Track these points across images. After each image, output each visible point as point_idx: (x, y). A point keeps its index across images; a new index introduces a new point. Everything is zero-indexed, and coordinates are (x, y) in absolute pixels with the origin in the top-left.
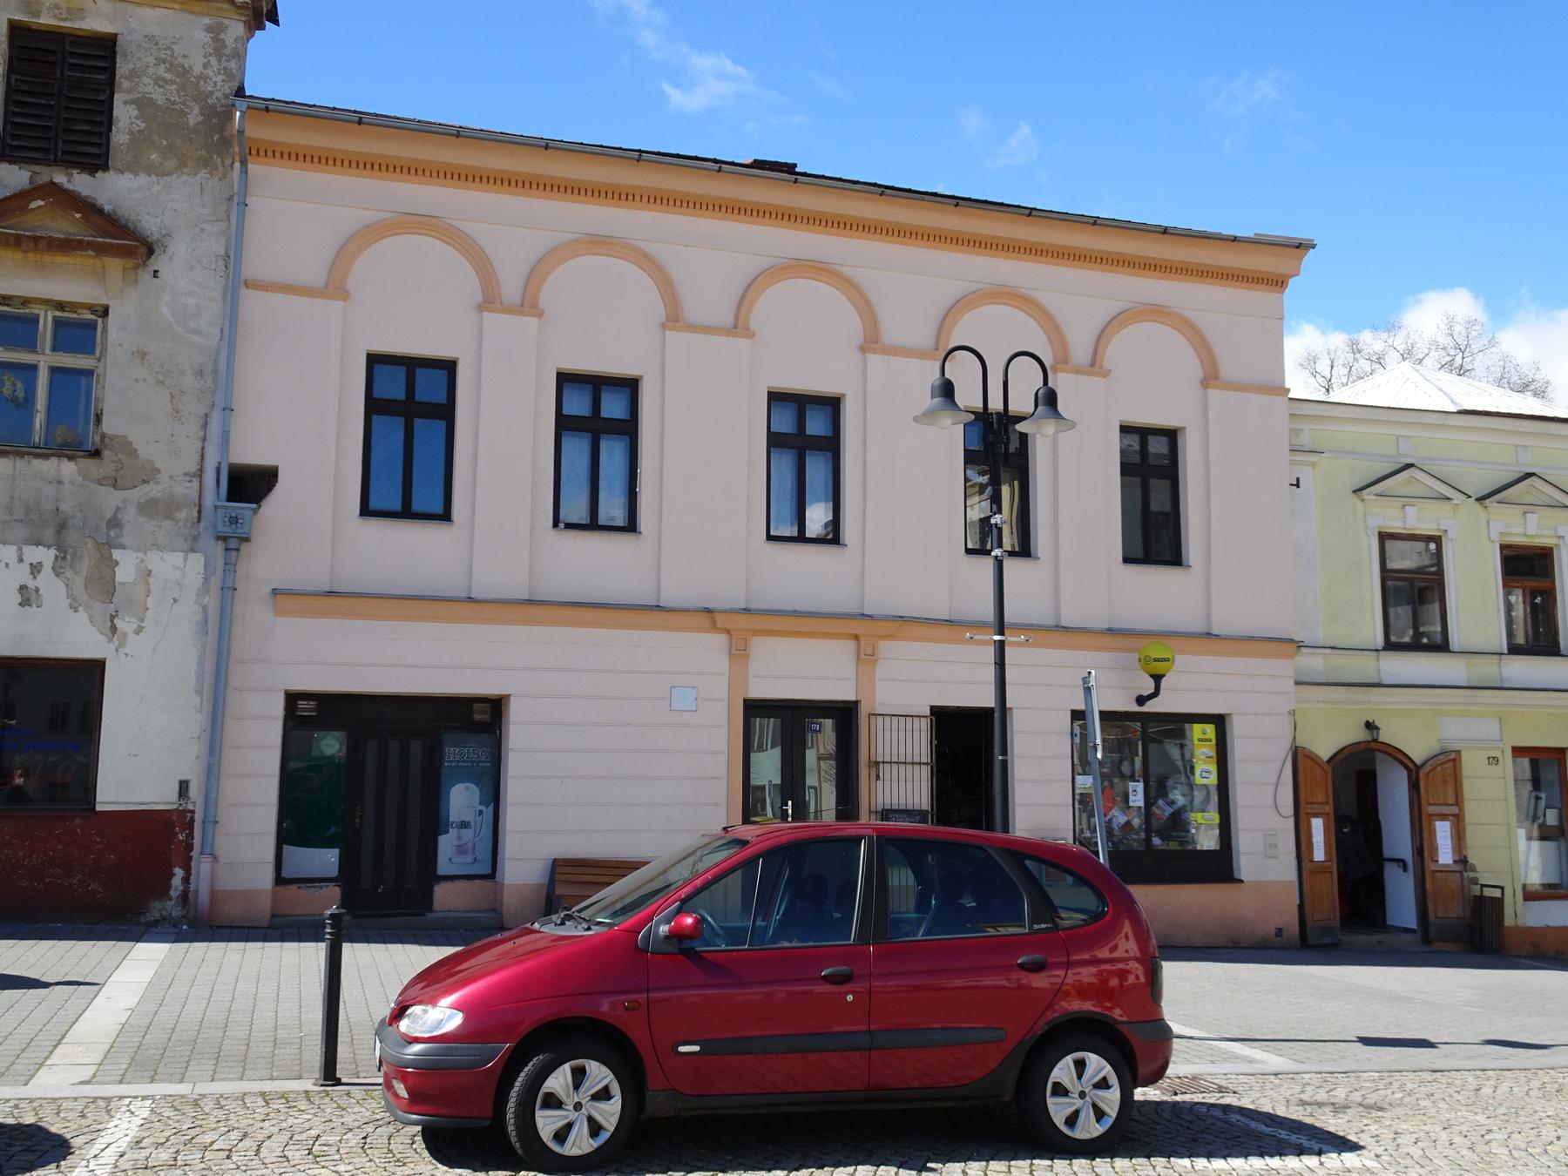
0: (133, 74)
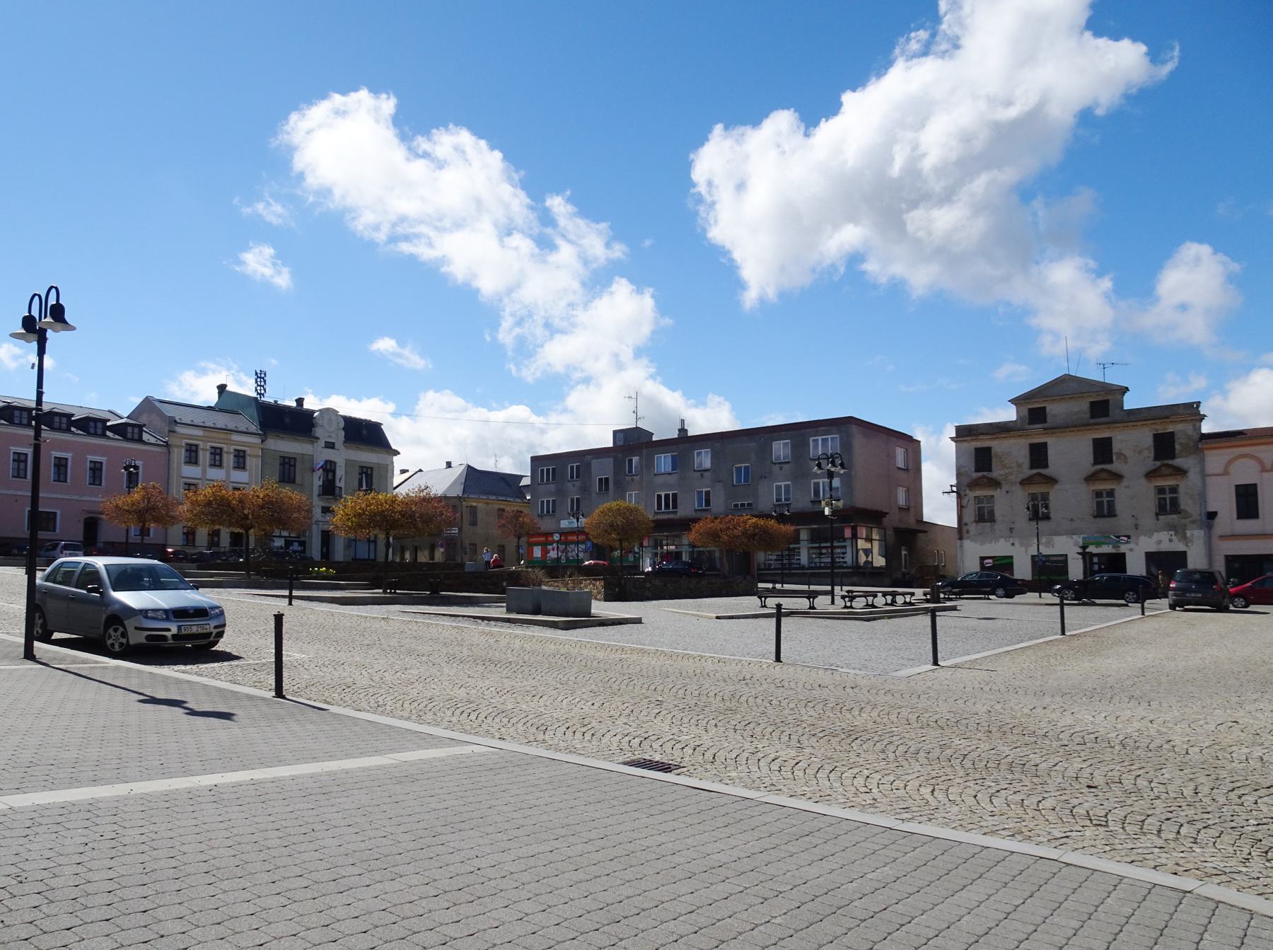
0: (1178, 439)
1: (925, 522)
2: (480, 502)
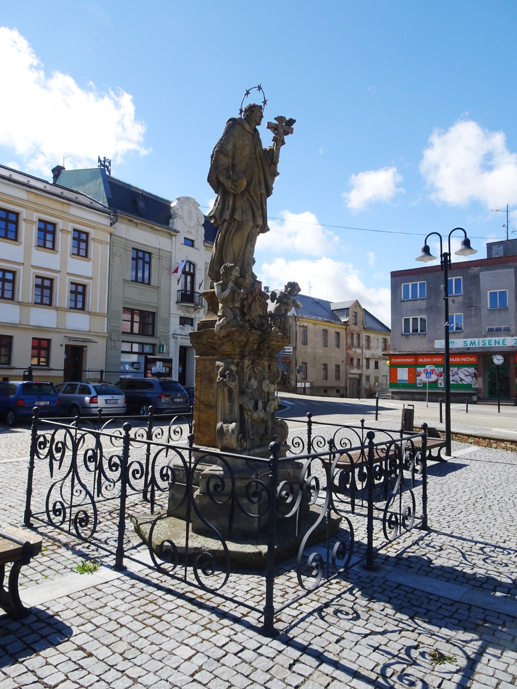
2: (310, 323)
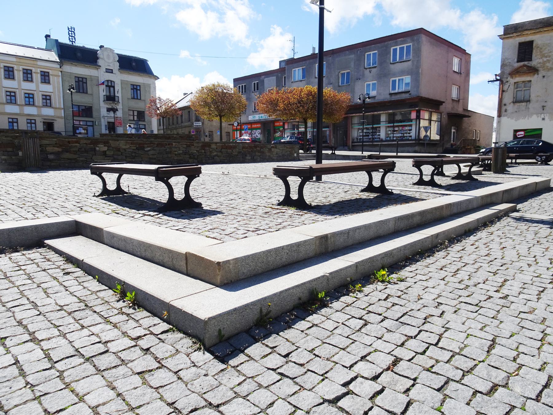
1: (470, 111)
